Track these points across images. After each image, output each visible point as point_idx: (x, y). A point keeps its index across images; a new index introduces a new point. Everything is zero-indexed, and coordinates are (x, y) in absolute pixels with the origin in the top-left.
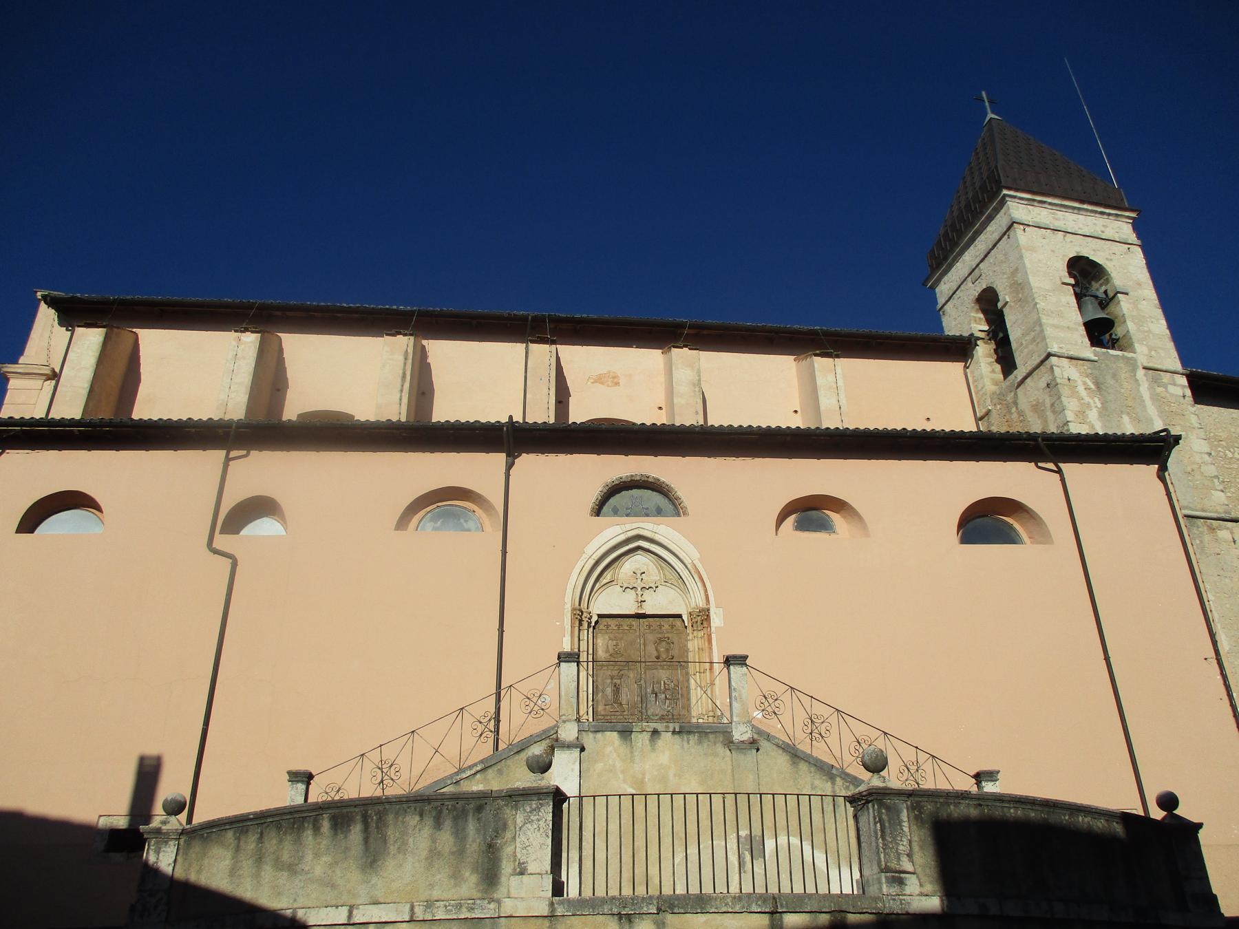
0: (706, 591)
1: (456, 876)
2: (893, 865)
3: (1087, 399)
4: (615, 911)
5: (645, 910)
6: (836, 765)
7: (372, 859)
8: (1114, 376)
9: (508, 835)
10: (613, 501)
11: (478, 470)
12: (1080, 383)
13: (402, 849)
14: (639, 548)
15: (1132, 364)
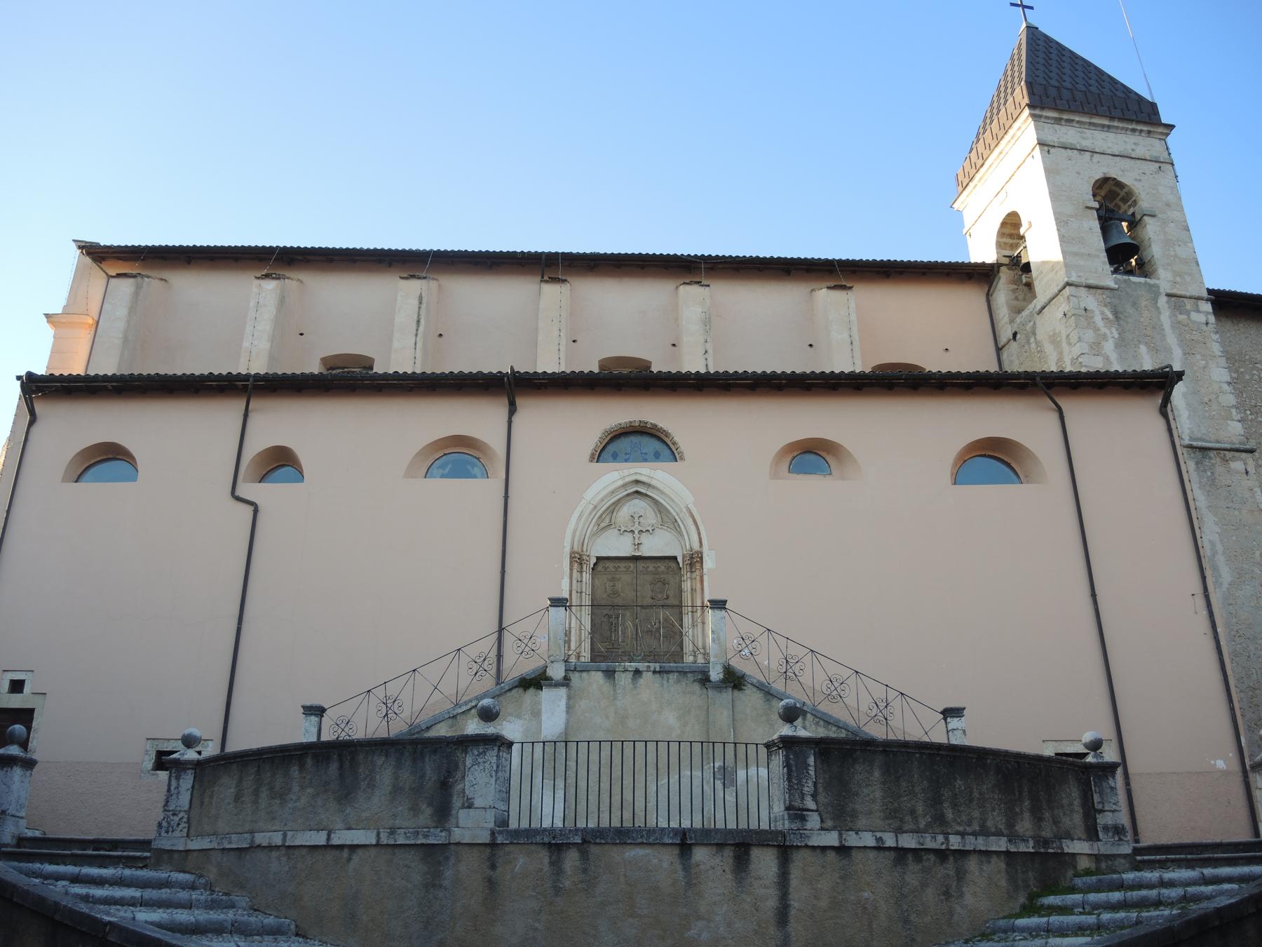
0: (699, 534)
1: (415, 810)
2: (797, 804)
3: (1104, 330)
4: (546, 840)
5: (571, 840)
6: (808, 702)
7: (346, 793)
8: (1134, 304)
9: (459, 775)
10: (611, 448)
11: (481, 419)
12: (1097, 312)
13: (372, 785)
14: (637, 492)
15: (1154, 291)
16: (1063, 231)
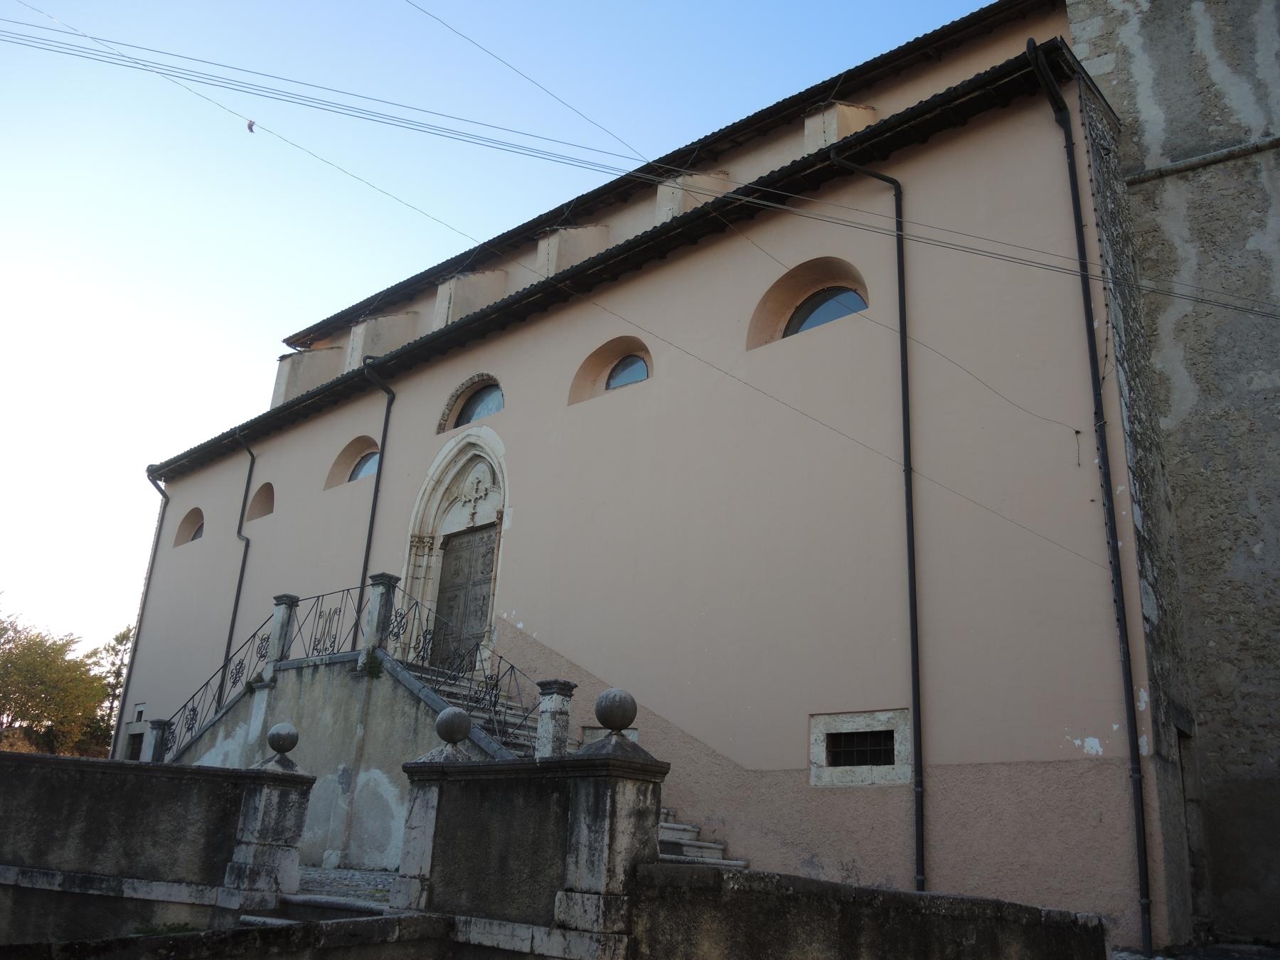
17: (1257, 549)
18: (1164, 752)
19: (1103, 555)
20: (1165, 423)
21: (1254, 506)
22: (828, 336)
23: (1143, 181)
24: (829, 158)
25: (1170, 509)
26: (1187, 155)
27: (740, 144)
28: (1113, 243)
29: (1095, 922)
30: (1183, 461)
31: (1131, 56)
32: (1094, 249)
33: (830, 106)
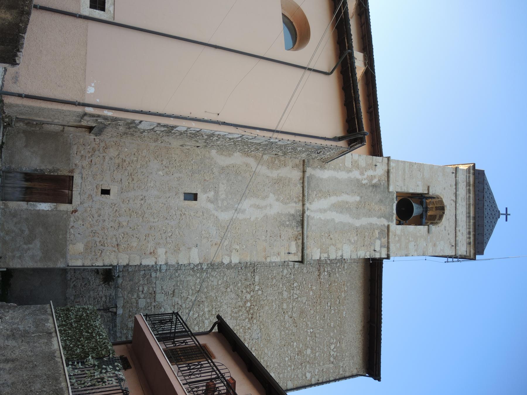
8: (381, 201)
16: (415, 167)
17: (161, 173)
18: (85, 118)
19: (169, 112)
20: (214, 152)
21: (177, 175)
22: (279, 33)
23: (303, 165)
24: (348, 49)
25: (181, 146)
26: (308, 182)
27: (361, 27)
28: (285, 146)
29: (18, 62)
30: (198, 155)
31: (348, 173)
32: (286, 137)
33: (365, 65)
